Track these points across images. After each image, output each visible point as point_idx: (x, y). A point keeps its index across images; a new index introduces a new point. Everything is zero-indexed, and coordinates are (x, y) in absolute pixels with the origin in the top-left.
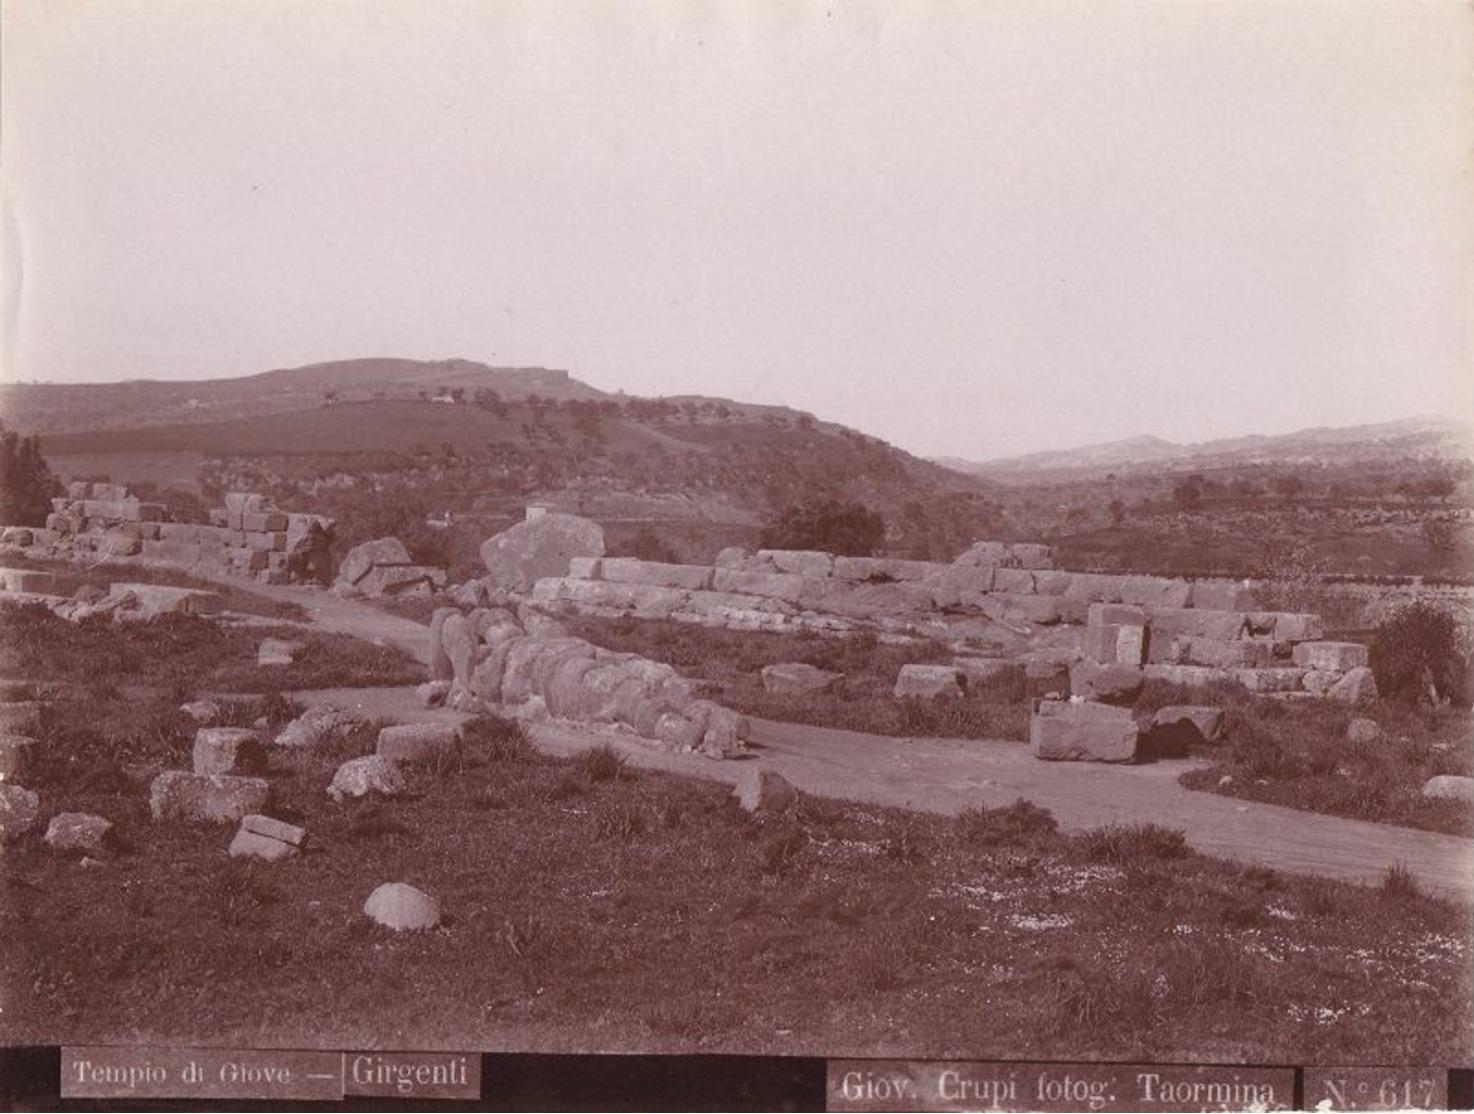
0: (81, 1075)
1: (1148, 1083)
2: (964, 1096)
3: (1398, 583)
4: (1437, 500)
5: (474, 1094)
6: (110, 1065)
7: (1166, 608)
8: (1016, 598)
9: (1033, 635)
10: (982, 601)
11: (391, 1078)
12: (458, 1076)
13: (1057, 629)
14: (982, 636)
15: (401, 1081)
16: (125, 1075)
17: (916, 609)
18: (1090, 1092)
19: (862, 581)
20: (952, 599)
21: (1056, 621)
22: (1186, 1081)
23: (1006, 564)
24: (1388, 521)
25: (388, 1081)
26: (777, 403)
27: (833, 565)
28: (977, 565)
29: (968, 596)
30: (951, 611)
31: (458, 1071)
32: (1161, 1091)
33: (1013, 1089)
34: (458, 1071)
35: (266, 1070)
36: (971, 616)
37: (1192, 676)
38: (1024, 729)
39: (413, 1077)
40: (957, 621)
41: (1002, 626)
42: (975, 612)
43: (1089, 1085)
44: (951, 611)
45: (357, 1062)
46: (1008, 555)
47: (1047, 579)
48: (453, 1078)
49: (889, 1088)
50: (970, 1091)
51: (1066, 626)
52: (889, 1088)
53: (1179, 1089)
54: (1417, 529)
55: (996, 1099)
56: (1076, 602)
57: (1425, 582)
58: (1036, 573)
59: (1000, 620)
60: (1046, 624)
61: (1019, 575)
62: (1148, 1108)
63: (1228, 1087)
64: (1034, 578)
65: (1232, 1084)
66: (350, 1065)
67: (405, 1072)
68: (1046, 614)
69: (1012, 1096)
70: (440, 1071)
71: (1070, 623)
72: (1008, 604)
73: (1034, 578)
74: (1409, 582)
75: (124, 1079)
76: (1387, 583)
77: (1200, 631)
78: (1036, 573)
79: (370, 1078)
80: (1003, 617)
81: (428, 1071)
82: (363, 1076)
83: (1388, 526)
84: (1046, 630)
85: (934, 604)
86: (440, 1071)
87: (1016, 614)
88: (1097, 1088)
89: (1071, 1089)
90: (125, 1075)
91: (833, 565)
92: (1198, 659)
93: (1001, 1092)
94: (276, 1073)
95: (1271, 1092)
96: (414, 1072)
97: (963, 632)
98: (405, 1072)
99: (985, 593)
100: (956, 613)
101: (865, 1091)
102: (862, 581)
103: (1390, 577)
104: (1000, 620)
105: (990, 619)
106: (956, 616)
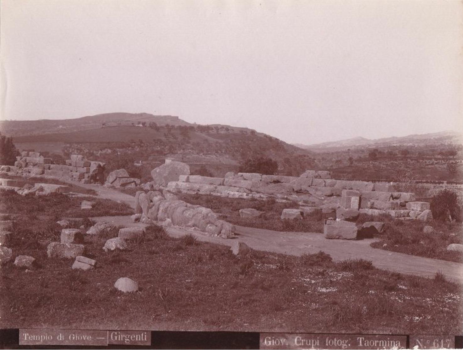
0: (25, 338)
1: (361, 340)
2: (303, 344)
3: (439, 183)
4: (451, 157)
5: (149, 344)
6: (35, 335)
7: (366, 191)
8: (319, 188)
9: (324, 199)
10: (308, 189)
11: (123, 339)
12: (144, 338)
13: (332, 198)
14: (308, 200)
15: (126, 340)
16: (39, 338)
17: (288, 191)
18: (342, 343)
19: (271, 183)
20: (299, 188)
21: (332, 195)
22: (373, 340)
23: (316, 177)
24: (436, 164)
25: (122, 340)
26: (244, 127)
27: (262, 178)
28: (307, 177)
29: (304, 187)
30: (299, 192)
31: (144, 336)
32: (365, 343)
33: (318, 342)
34: (144, 336)
35: (84, 336)
36: (305, 194)
37: (374, 212)
38: (322, 229)
39: (130, 339)
40: (301, 195)
41: (315, 197)
42: (306, 192)
43: (342, 341)
44: (299, 192)
45: (112, 334)
46: (317, 174)
47: (329, 182)
48: (142, 339)
49: (279, 342)
50: (305, 343)
51: (335, 197)
52: (279, 342)
53: (370, 342)
54: (445, 166)
55: (313, 345)
56: (338, 189)
57: (448, 183)
58: (325, 180)
59: (314, 195)
60: (329, 196)
61: (320, 181)
62: (361, 348)
63: (386, 342)
64: (325, 181)
65: (387, 340)
66: (110, 335)
67: (127, 337)
68: (329, 193)
69: (318, 344)
70: (138, 336)
71: (336, 196)
72: (317, 190)
73: (325, 181)
74: (443, 183)
75: (39, 339)
76: (436, 183)
77: (377, 198)
78: (325, 180)
79: (116, 339)
80: (315, 194)
81: (134, 336)
82: (114, 338)
83: (436, 165)
84: (329, 198)
85: (293, 190)
86: (138, 336)
87: (319, 193)
88: (345, 342)
89: (336, 342)
90: (39, 338)
91: (262, 178)
92: (376, 207)
93: (314, 343)
94: (87, 337)
95: (399, 343)
96: (130, 337)
97: (302, 198)
98: (127, 337)
99: (309, 186)
100: (300, 193)
101: (272, 343)
102: (271, 183)
103: (437, 181)
104: (314, 195)
105: (311, 195)
106: (300, 194)
